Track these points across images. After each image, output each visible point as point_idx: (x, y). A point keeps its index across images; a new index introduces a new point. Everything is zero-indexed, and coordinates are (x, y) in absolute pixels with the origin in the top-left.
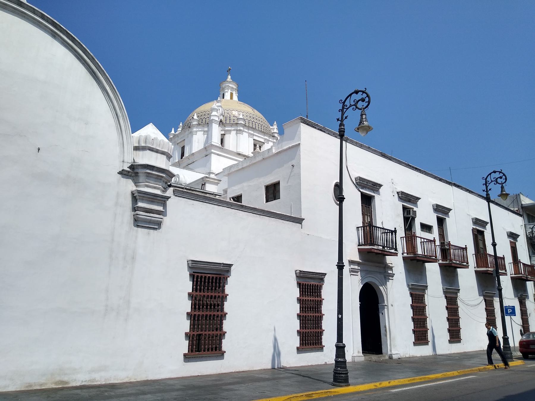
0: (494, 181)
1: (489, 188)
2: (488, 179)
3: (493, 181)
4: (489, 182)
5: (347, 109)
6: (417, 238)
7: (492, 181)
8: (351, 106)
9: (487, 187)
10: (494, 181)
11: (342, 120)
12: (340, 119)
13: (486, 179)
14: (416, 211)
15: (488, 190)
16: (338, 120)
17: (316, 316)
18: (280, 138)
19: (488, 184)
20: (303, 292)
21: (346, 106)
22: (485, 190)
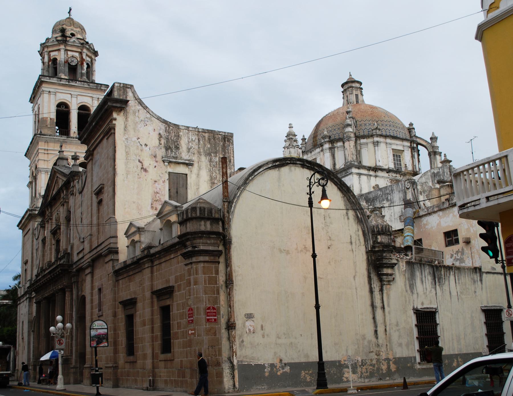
0: (317, 182)
1: (312, 191)
2: (312, 180)
3: (316, 183)
4: (312, 183)
5: (313, 185)
6: (392, 166)
7: (315, 182)
8: (315, 183)
9: (310, 189)
10: (317, 182)
11: (310, 195)
12: (309, 193)
13: (310, 180)
14: (438, 147)
15: (312, 193)
16: (308, 194)
17: (428, 335)
18: (64, 352)
19: (311, 186)
20: (420, 320)
21: (317, 185)
22: (309, 193)
